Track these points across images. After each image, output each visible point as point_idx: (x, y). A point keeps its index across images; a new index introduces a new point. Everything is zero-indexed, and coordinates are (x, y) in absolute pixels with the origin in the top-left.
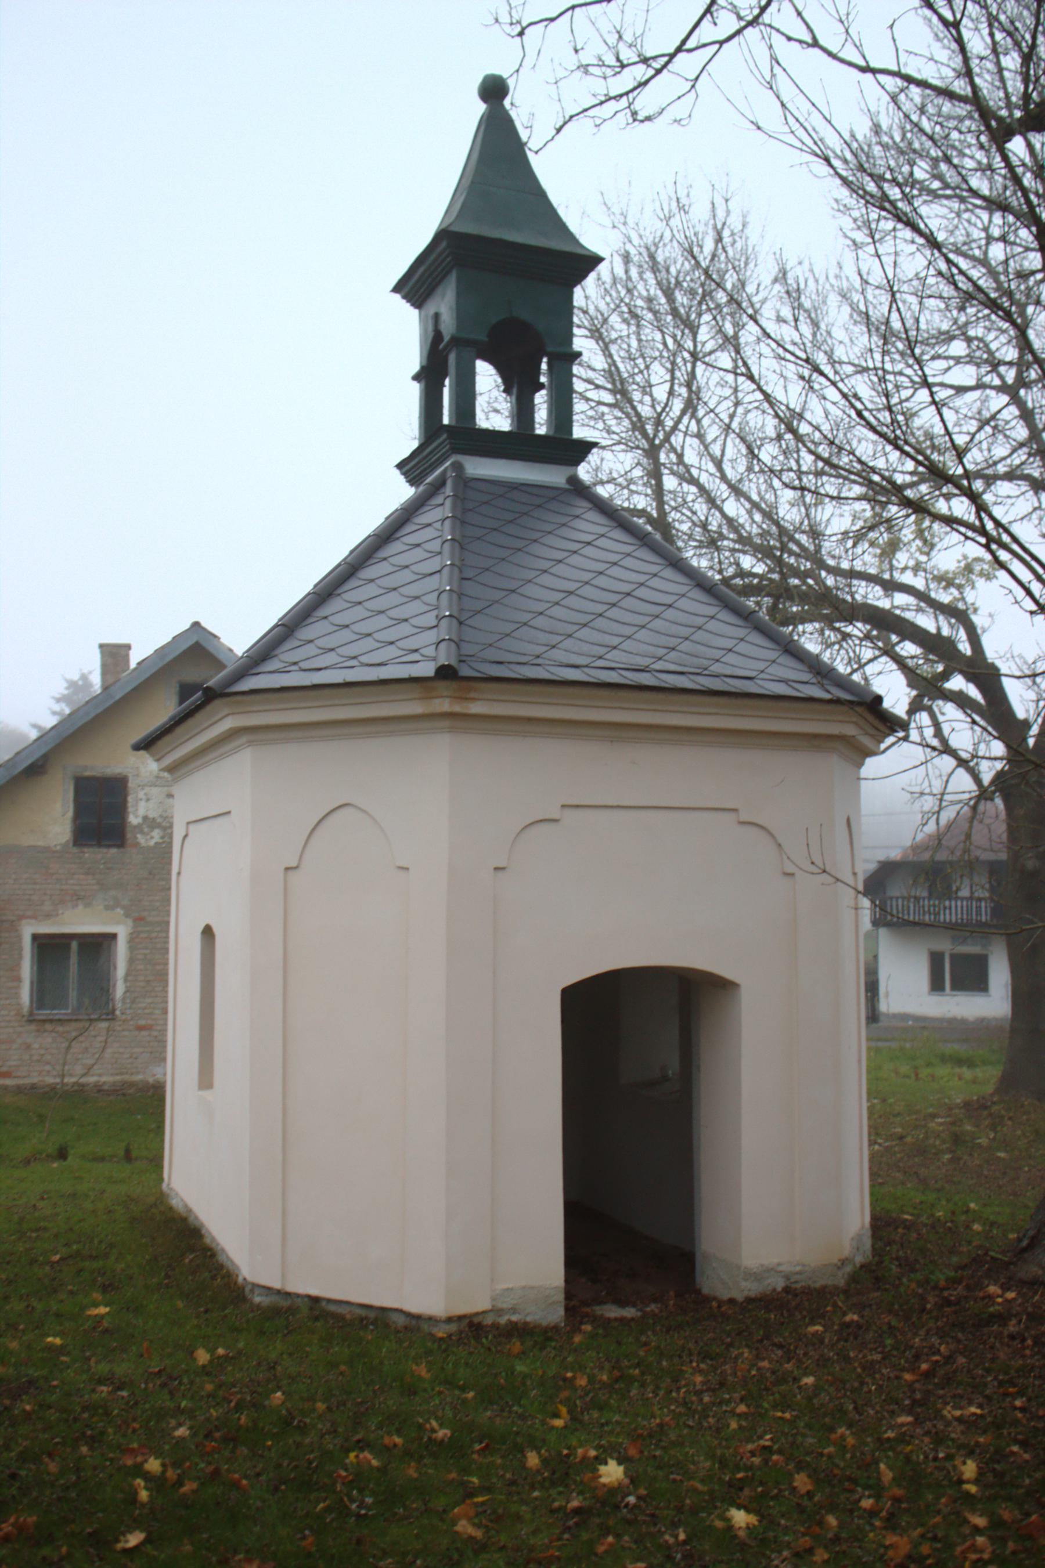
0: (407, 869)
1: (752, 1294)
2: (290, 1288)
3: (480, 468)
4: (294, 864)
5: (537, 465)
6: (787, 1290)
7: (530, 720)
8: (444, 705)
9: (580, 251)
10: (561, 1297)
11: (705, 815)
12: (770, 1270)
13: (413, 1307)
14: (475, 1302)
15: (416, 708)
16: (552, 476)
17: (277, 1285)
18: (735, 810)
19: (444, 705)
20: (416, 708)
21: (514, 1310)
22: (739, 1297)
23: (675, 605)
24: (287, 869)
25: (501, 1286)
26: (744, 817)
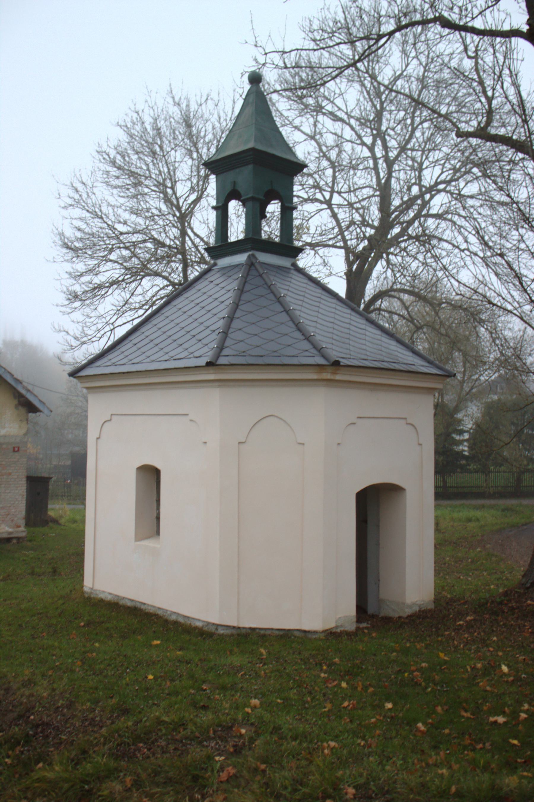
0: (303, 444)
1: (409, 614)
2: (241, 625)
3: (264, 257)
4: (244, 441)
5: (281, 257)
6: (419, 611)
7: (350, 382)
8: (329, 376)
9: (295, 160)
10: (355, 620)
11: (396, 421)
12: (414, 604)
13: (306, 627)
14: (331, 624)
15: (315, 376)
16: (284, 262)
17: (235, 624)
18: (405, 419)
19: (329, 376)
20: (315, 376)
21: (341, 626)
22: (405, 615)
23: (282, 310)
24: (239, 443)
25: (338, 616)
26: (409, 422)
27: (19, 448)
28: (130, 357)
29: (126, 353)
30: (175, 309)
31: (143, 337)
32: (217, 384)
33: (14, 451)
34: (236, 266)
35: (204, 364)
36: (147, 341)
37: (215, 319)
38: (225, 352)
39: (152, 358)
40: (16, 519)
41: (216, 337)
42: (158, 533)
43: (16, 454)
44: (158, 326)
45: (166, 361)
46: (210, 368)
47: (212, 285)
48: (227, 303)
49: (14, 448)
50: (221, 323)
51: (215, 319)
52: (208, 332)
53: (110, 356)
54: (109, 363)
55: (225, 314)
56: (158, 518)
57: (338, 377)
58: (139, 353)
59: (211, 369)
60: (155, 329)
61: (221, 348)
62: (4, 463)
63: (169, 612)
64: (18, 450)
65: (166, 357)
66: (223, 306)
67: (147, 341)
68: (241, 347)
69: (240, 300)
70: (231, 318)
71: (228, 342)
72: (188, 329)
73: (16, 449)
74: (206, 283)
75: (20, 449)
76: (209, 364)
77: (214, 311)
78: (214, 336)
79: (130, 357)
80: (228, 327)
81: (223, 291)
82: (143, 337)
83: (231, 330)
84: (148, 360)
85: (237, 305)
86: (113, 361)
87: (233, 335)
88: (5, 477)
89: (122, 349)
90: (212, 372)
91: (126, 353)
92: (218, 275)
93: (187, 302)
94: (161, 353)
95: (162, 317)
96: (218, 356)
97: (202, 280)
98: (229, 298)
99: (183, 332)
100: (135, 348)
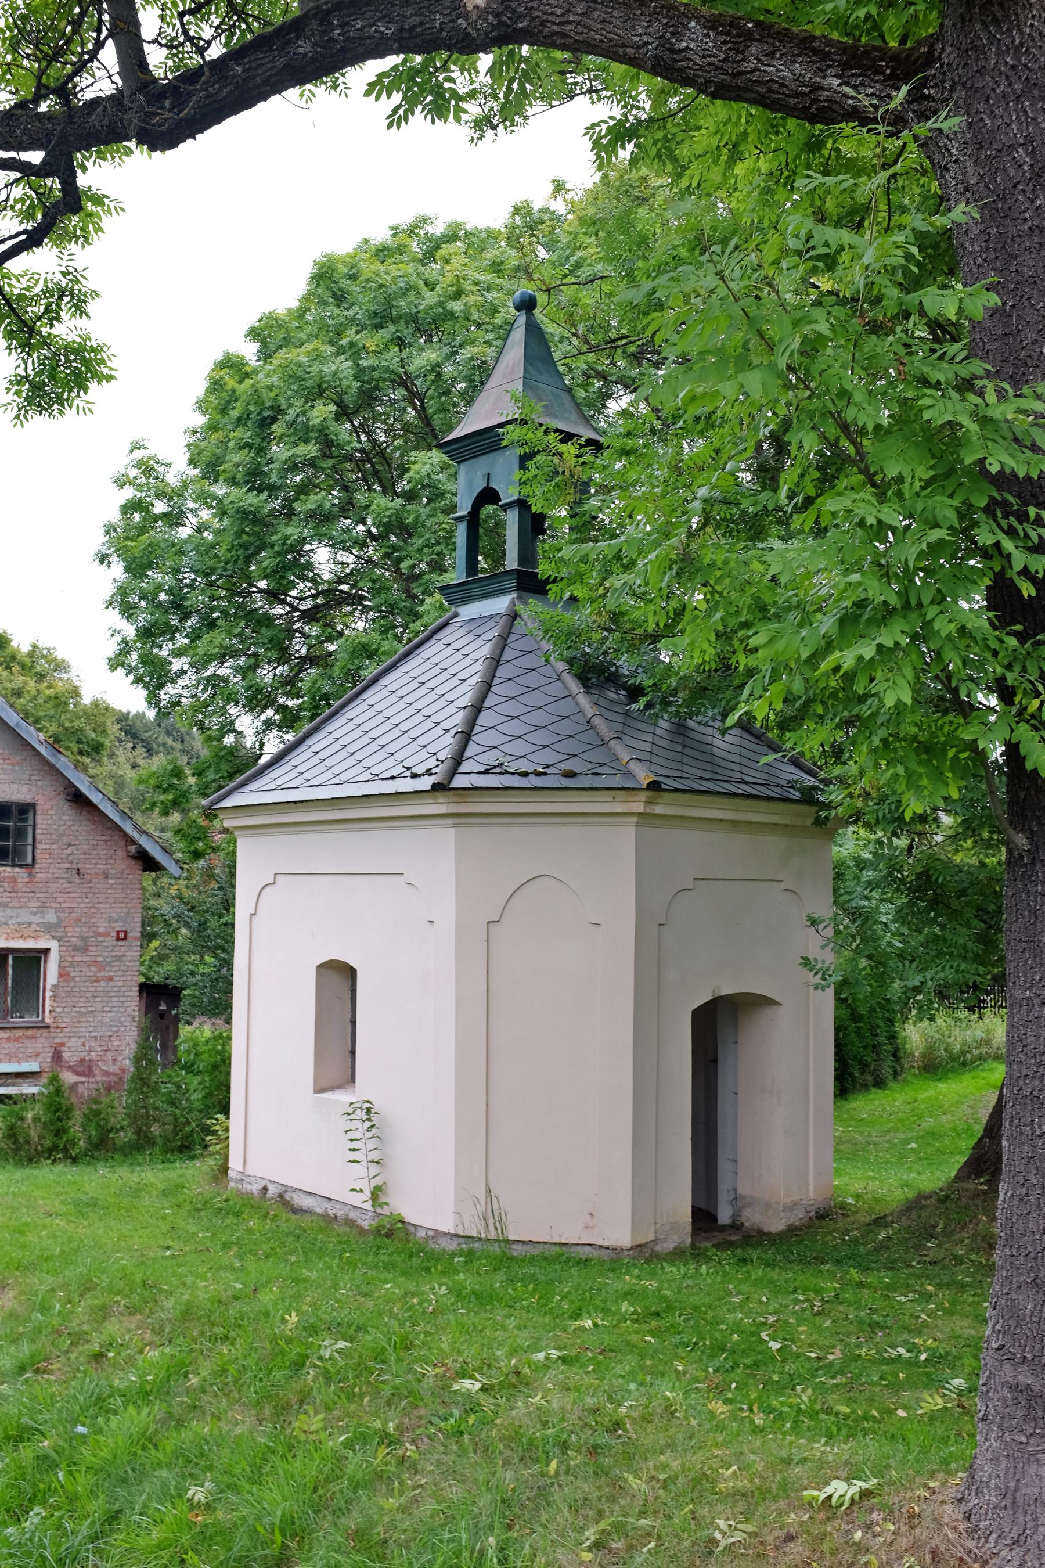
27: (126, 933)
28: (307, 776)
29: (300, 769)
30: (385, 692)
31: (330, 739)
32: (450, 821)
33: (118, 939)
34: (491, 617)
35: (429, 788)
36: (336, 747)
37: (452, 709)
38: (465, 767)
39: (344, 777)
40: (120, 1058)
41: (451, 740)
42: (353, 1080)
43: (121, 943)
44: (357, 721)
45: (393, 778)
46: (437, 794)
47: (449, 651)
48: (473, 681)
49: (118, 932)
50: (459, 718)
51: (452, 709)
52: (438, 731)
53: (274, 774)
54: (272, 786)
55: (466, 701)
56: (353, 1053)
57: (659, 809)
58: (322, 767)
59: (441, 797)
60: (351, 726)
61: (458, 759)
62: (100, 959)
63: (422, 1234)
64: (125, 939)
65: (367, 776)
66: (465, 687)
67: (336, 747)
68: (492, 758)
69: (494, 676)
70: (477, 709)
71: (471, 750)
72: (404, 727)
73: (122, 936)
74: (440, 646)
75: (129, 935)
76: (436, 787)
77: (450, 697)
78: (449, 739)
79: (307, 776)
80: (472, 722)
81: (468, 661)
82: (330, 739)
83: (477, 729)
84: (336, 780)
85: (490, 686)
86: (279, 782)
87: (481, 737)
88: (102, 984)
89: (294, 762)
90: (442, 800)
91: (300, 769)
92: (461, 632)
93: (406, 679)
94: (359, 768)
95: (364, 706)
96: (453, 772)
97: (432, 642)
98: (475, 672)
99: (396, 732)
100: (316, 760)
